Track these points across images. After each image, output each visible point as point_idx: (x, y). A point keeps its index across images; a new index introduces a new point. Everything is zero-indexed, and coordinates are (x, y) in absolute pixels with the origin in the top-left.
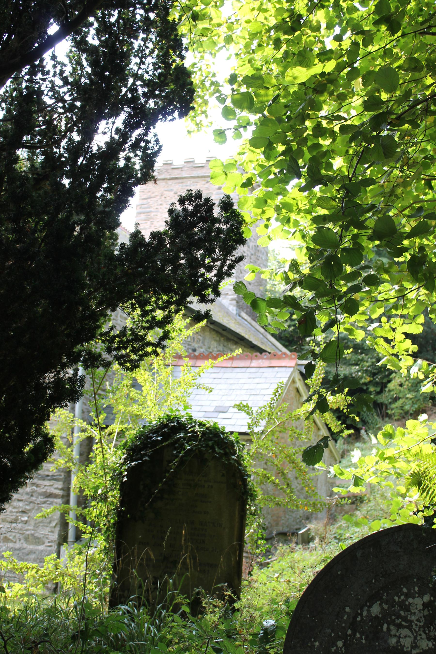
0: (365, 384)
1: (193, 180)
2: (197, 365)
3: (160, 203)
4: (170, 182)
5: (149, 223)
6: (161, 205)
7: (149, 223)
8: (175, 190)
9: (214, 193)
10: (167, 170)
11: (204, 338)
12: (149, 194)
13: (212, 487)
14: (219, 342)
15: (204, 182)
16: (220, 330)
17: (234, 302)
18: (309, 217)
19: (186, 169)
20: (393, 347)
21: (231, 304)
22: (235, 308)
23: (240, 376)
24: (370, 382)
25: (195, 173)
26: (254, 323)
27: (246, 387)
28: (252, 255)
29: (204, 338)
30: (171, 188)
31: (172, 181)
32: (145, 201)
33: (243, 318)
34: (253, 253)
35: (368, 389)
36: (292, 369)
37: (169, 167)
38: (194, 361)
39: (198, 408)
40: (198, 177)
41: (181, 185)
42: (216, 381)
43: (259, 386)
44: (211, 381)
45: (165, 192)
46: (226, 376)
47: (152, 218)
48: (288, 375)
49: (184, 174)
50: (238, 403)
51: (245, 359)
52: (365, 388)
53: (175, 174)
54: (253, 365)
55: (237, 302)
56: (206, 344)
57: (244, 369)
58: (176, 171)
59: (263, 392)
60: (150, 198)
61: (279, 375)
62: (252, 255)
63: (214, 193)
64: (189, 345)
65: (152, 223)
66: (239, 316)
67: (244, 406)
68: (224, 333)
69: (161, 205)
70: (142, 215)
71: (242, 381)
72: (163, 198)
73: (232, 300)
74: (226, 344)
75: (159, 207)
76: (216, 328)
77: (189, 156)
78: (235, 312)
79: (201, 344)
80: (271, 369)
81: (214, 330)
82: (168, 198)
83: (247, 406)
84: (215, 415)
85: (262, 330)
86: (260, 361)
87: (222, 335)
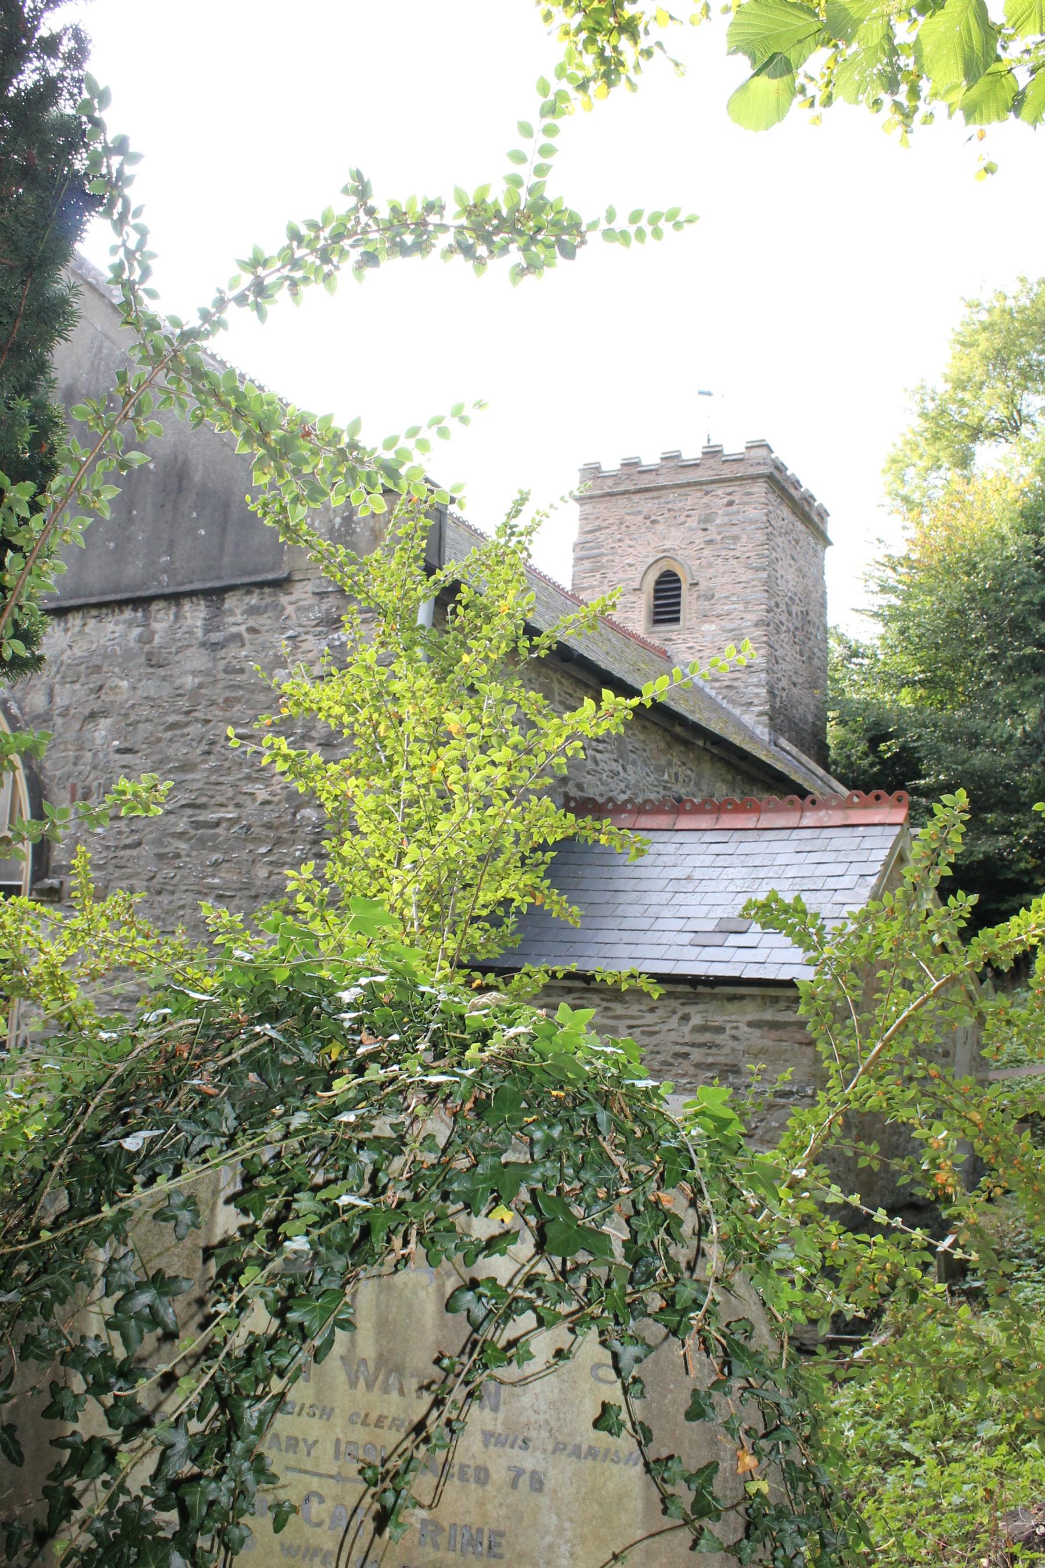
0: (1026, 872)
1: (679, 491)
2: (678, 826)
4: (636, 498)
5: (598, 575)
7: (598, 575)
8: (646, 511)
10: (629, 477)
11: (700, 776)
13: (537, 1483)
14: (732, 785)
16: (734, 759)
17: (765, 718)
18: (695, 1294)
22: (766, 730)
23: (776, 847)
24: (1036, 867)
25: (682, 479)
26: (804, 758)
27: (791, 872)
29: (700, 776)
32: (590, 537)
35: (1032, 880)
36: (898, 829)
37: (633, 470)
38: (673, 817)
39: (679, 924)
40: (689, 485)
42: (721, 861)
43: (822, 870)
44: (708, 860)
46: (744, 848)
48: (890, 844)
49: (662, 481)
50: (761, 897)
51: (787, 810)
52: (1026, 880)
53: (645, 482)
54: (805, 822)
55: (771, 719)
56: (704, 787)
57: (784, 834)
59: (832, 883)
60: (599, 529)
61: (867, 843)
64: (665, 788)
67: (786, 910)
68: (743, 765)
71: (781, 860)
73: (761, 714)
74: (747, 788)
76: (724, 754)
77: (670, 447)
78: (766, 738)
79: (692, 787)
80: (848, 831)
81: (721, 759)
83: (797, 909)
84: (718, 939)
85: (821, 772)
86: (822, 813)
87: (738, 771)
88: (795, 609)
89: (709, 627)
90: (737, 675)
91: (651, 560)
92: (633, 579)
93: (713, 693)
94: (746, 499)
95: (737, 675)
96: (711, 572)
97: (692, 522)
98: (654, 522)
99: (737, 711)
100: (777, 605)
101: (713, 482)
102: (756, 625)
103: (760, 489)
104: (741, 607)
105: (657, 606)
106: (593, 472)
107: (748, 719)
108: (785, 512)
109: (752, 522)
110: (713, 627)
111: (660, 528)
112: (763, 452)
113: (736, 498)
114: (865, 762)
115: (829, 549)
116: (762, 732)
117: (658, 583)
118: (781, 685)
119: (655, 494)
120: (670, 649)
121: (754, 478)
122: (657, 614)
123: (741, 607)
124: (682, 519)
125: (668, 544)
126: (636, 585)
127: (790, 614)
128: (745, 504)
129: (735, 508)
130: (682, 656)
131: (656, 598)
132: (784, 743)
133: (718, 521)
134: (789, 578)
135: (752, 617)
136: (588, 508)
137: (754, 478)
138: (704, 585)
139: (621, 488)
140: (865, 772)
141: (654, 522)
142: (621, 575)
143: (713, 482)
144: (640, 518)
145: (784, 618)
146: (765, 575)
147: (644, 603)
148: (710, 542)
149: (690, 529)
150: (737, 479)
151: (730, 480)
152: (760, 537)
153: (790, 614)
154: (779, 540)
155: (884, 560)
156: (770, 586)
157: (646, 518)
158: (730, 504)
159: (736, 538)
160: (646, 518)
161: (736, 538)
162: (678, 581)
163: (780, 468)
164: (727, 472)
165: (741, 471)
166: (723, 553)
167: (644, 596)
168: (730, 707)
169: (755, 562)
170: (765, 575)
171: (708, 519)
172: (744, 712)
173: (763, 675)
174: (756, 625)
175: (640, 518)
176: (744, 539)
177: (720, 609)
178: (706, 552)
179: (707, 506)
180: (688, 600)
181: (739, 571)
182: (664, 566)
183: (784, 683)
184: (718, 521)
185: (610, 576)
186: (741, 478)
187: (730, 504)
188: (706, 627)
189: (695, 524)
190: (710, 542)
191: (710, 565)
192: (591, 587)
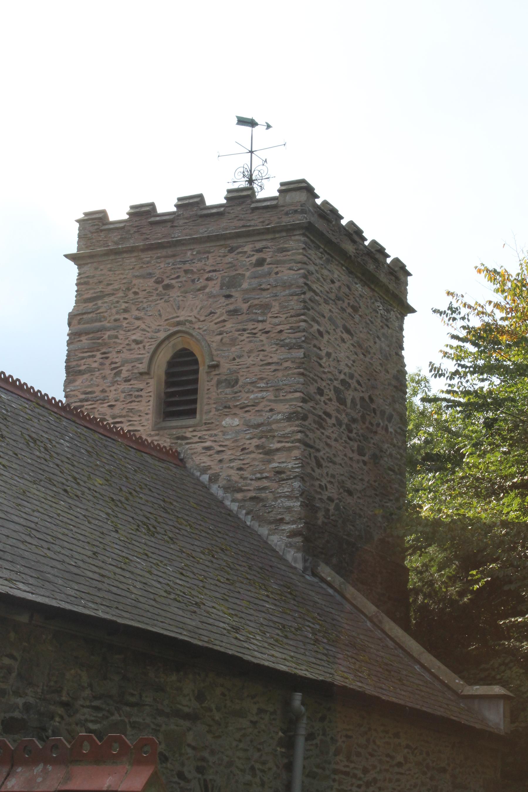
1: (198, 247)
3: (124, 306)
4: (146, 256)
6: (126, 311)
7: (99, 355)
9: (248, 274)
12: (100, 288)
15: (223, 251)
17: (298, 540)
19: (181, 222)
20: (460, 313)
21: (290, 545)
25: (202, 231)
28: (354, 420)
30: (150, 271)
31: (150, 253)
33: (323, 580)
34: (357, 416)
40: (209, 239)
41: (171, 260)
45: (135, 281)
47: (105, 344)
49: (178, 235)
53: (158, 235)
55: (307, 540)
58: (160, 230)
60: (101, 296)
62: (354, 420)
63: (248, 274)
65: (105, 356)
66: (314, 574)
69: (126, 311)
70: (83, 338)
72: (131, 295)
73: (293, 534)
75: (121, 317)
78: (300, 566)
82: (142, 294)
88: (349, 395)
89: (231, 422)
90: (265, 483)
91: (162, 335)
92: (139, 360)
93: (234, 507)
94: (280, 257)
95: (265, 483)
96: (235, 350)
97: (214, 288)
98: (168, 287)
99: (264, 531)
100: (320, 392)
101: (238, 235)
102: (289, 419)
103: (295, 243)
104: (270, 395)
105: (168, 395)
106: (94, 225)
107: (277, 541)
108: (337, 273)
109: (286, 285)
110: (236, 421)
111: (175, 294)
112: (302, 197)
113: (268, 256)
114: (453, 590)
115: (409, 319)
116: (294, 557)
117: (171, 364)
118: (325, 495)
119: (170, 251)
120: (183, 449)
121: (290, 229)
122: (168, 404)
123: (270, 395)
124: (202, 282)
125: (183, 315)
126: (142, 367)
127: (342, 401)
128: (277, 263)
129: (266, 268)
130: (197, 459)
131: (168, 384)
132: (326, 571)
133: (245, 285)
134: (340, 355)
135: (284, 408)
136: (89, 269)
137: (290, 229)
138: (225, 367)
139: (130, 243)
140: (453, 603)
141: (168, 287)
142: (126, 355)
143: (238, 235)
144: (151, 282)
145: (331, 409)
146: (300, 353)
147: (151, 391)
148: (234, 312)
149: (211, 296)
150: (268, 231)
151: (259, 233)
152: (295, 304)
153: (342, 401)
154: (325, 309)
155: (463, 334)
156: (308, 367)
157: (157, 282)
158: (260, 263)
159: (266, 307)
160: (157, 282)
161: (266, 307)
162: (196, 362)
163: (329, 214)
164: (256, 222)
165: (274, 220)
166: (250, 326)
167: (152, 382)
168: (255, 525)
169: (289, 338)
170: (300, 353)
171: (232, 283)
172: (273, 532)
173: (296, 484)
174: (289, 419)
175: (151, 282)
176: (276, 307)
177: (246, 397)
178: (229, 325)
179: (232, 266)
180: (208, 389)
181: (267, 348)
182: (178, 343)
183: (332, 491)
184: (245, 285)
185: (113, 356)
186: (273, 231)
187: (260, 263)
188: (227, 421)
189: (216, 290)
190: (234, 312)
191: (233, 342)
192: (90, 370)
